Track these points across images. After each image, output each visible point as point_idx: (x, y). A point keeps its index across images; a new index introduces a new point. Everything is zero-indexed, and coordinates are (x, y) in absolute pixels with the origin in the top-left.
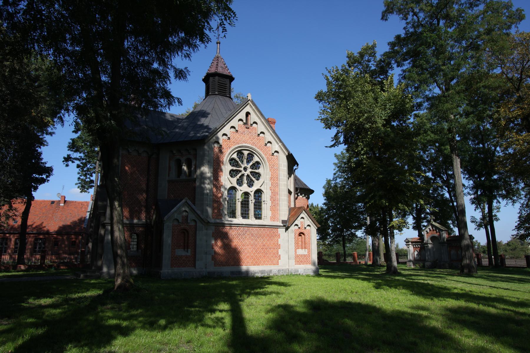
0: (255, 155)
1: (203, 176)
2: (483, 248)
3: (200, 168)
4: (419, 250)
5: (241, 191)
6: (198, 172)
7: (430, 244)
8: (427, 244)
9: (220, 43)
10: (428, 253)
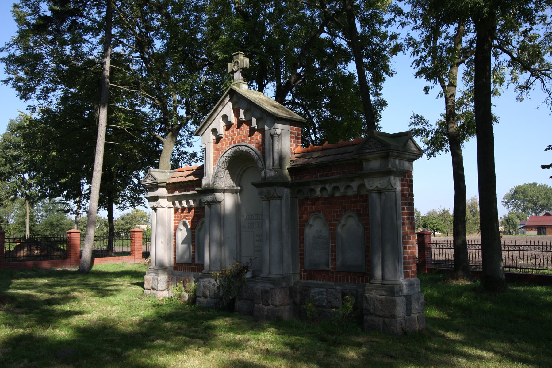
2: (424, 221)
4: (193, 222)
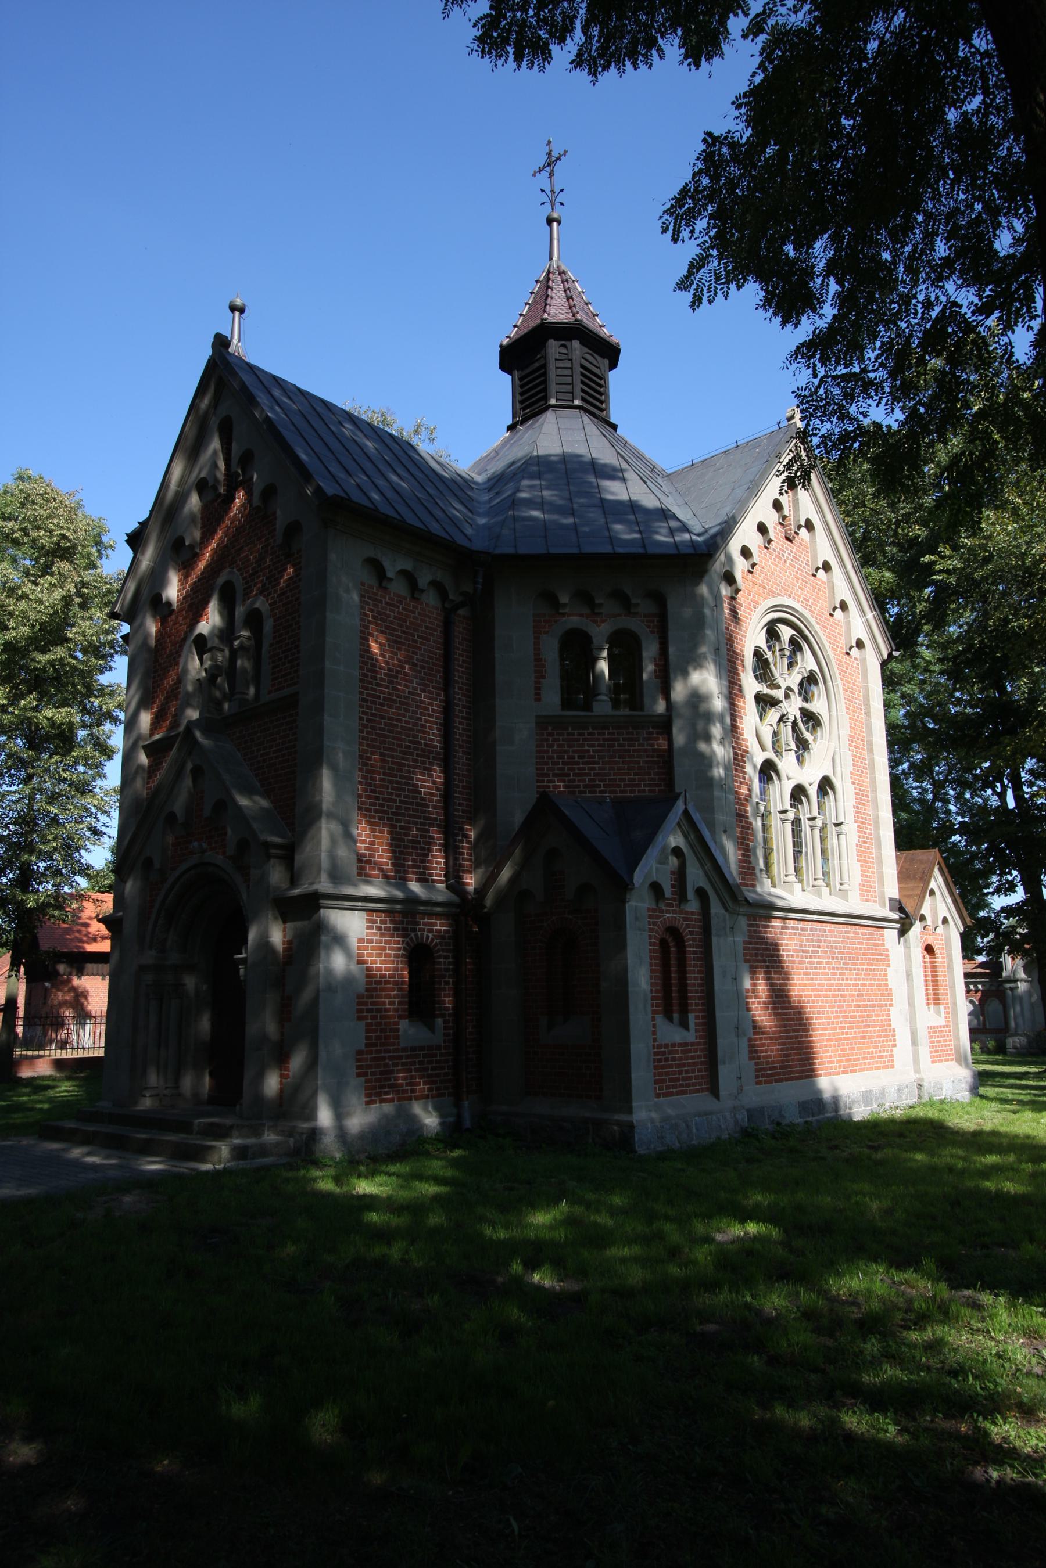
0: (805, 647)
1: (703, 707)
3: (685, 674)
4: (980, 1000)
5: (789, 779)
6: (679, 691)
7: (1022, 980)
8: (1016, 981)
9: (242, 311)
10: (1018, 1009)
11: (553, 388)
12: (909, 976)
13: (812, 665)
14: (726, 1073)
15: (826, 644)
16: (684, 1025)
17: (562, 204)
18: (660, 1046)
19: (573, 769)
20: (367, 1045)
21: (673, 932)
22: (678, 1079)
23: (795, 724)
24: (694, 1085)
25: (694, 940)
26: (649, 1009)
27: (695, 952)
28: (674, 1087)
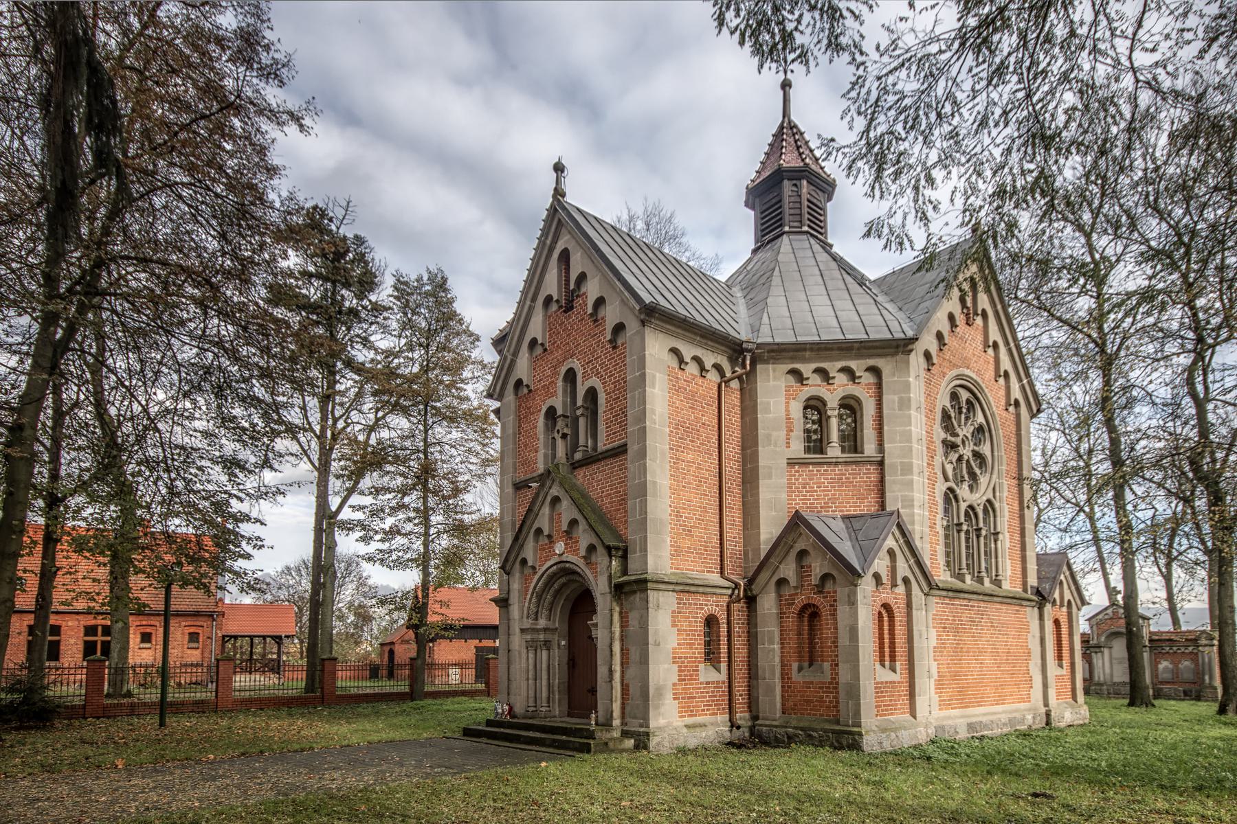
11: (787, 218)
12: (1042, 640)
13: (980, 419)
14: (921, 702)
15: (993, 403)
16: (893, 670)
17: (792, 71)
18: (877, 683)
19: (813, 496)
20: (679, 680)
21: (886, 606)
22: (889, 705)
23: (968, 461)
24: (900, 709)
25: (900, 612)
26: (872, 658)
27: (901, 621)
28: (887, 710)
